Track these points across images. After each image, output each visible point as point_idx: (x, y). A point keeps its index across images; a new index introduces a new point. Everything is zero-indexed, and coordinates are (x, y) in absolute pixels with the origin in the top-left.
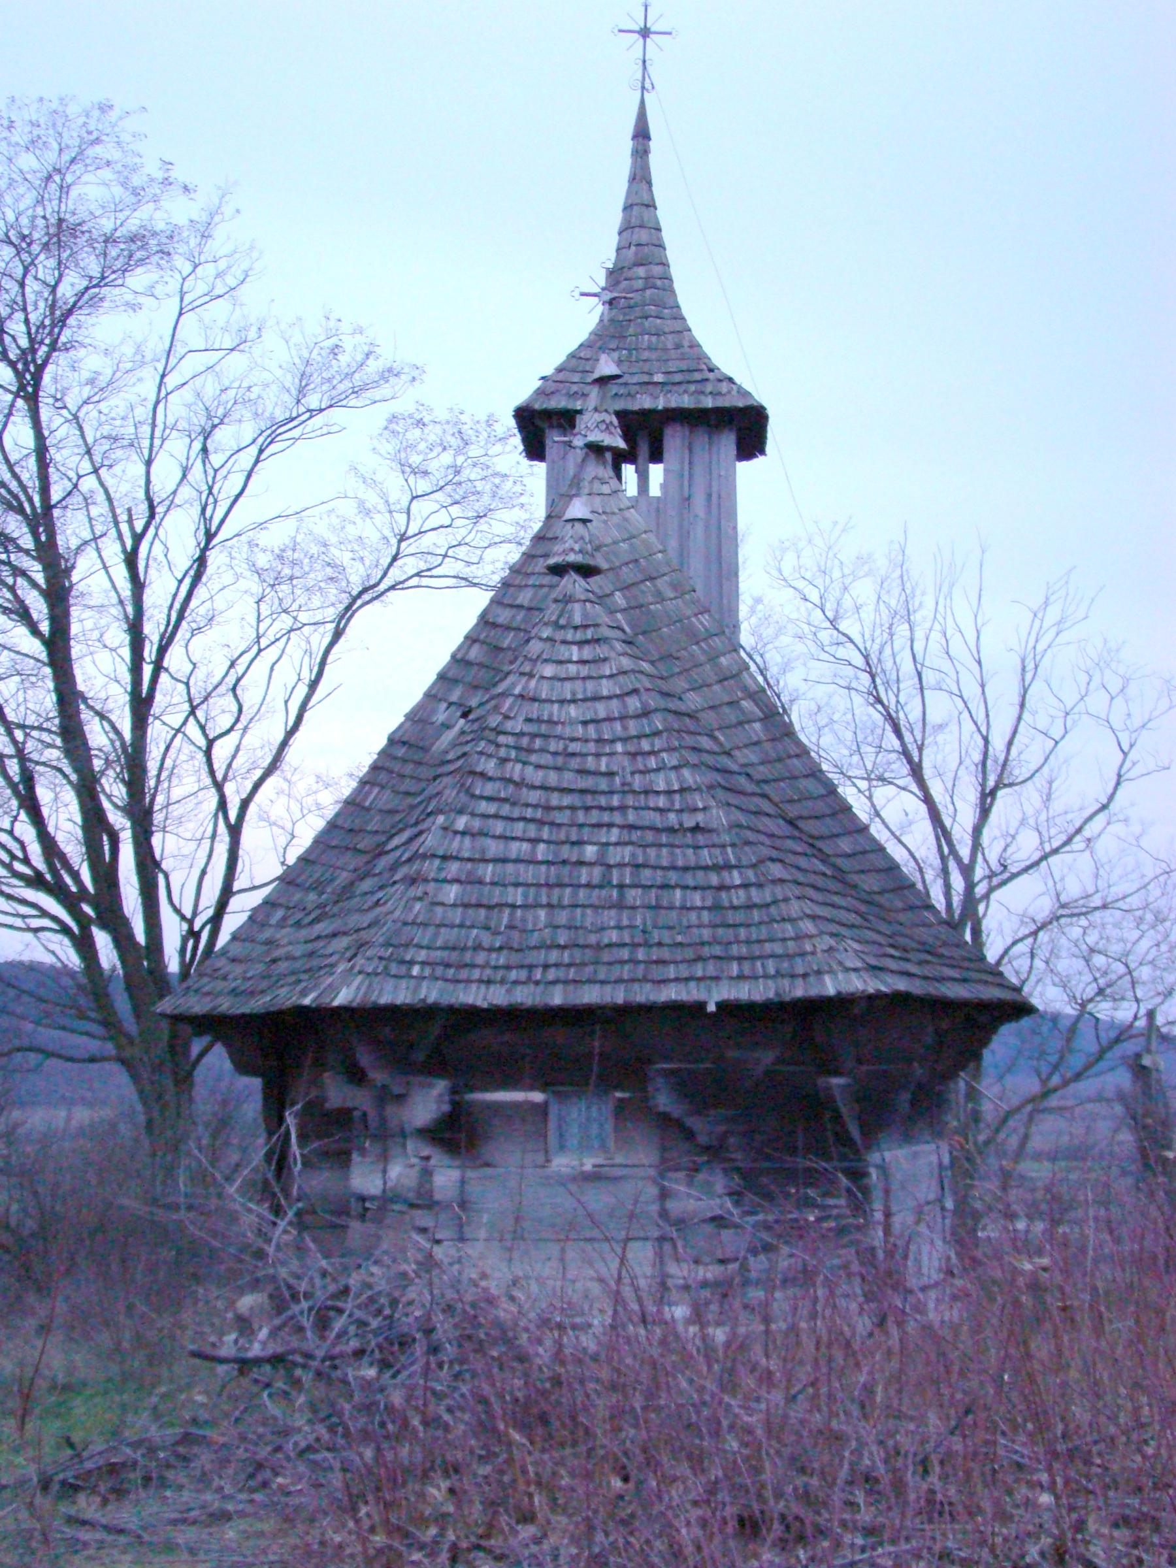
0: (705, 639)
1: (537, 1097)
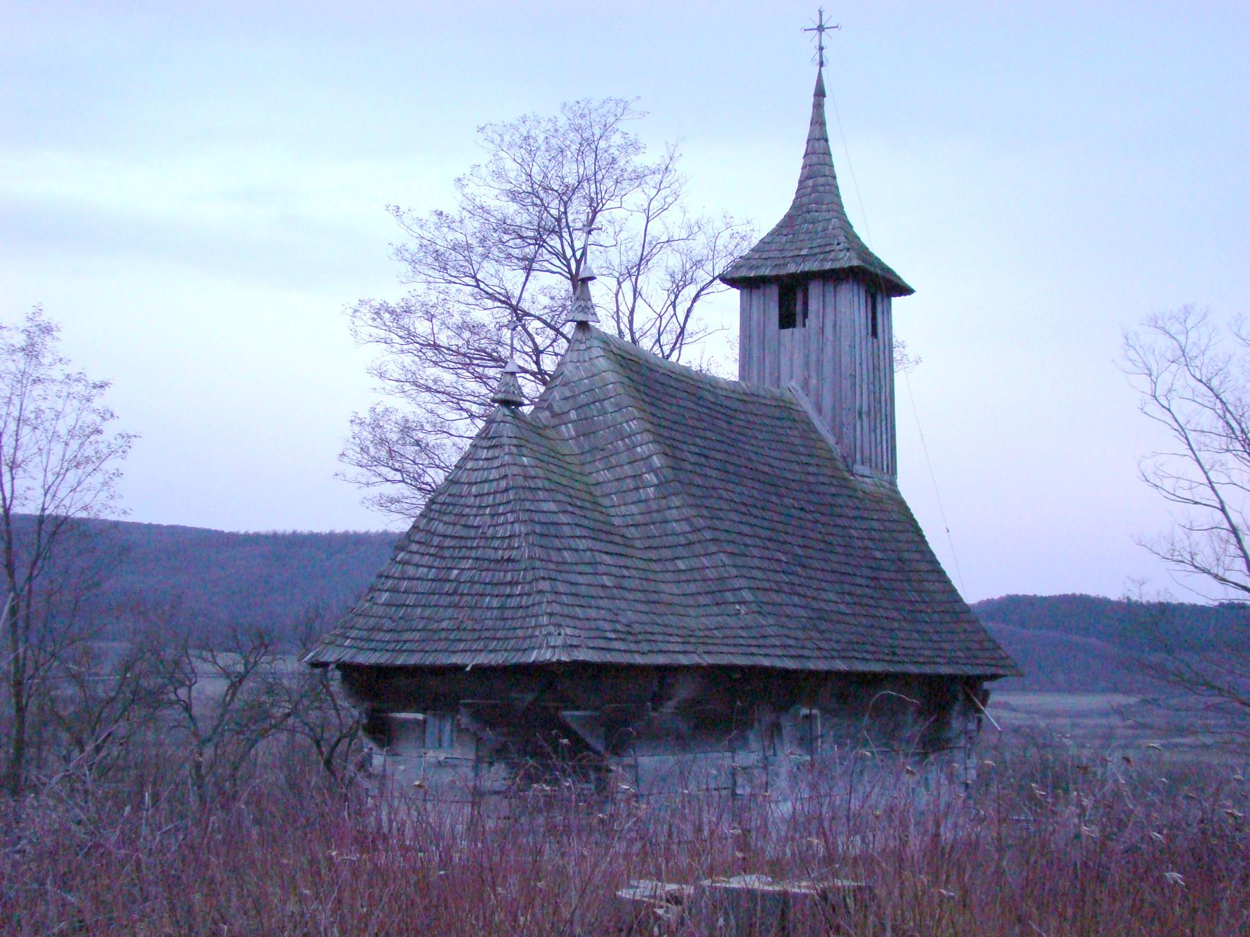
0: (629, 436)
1: (420, 716)
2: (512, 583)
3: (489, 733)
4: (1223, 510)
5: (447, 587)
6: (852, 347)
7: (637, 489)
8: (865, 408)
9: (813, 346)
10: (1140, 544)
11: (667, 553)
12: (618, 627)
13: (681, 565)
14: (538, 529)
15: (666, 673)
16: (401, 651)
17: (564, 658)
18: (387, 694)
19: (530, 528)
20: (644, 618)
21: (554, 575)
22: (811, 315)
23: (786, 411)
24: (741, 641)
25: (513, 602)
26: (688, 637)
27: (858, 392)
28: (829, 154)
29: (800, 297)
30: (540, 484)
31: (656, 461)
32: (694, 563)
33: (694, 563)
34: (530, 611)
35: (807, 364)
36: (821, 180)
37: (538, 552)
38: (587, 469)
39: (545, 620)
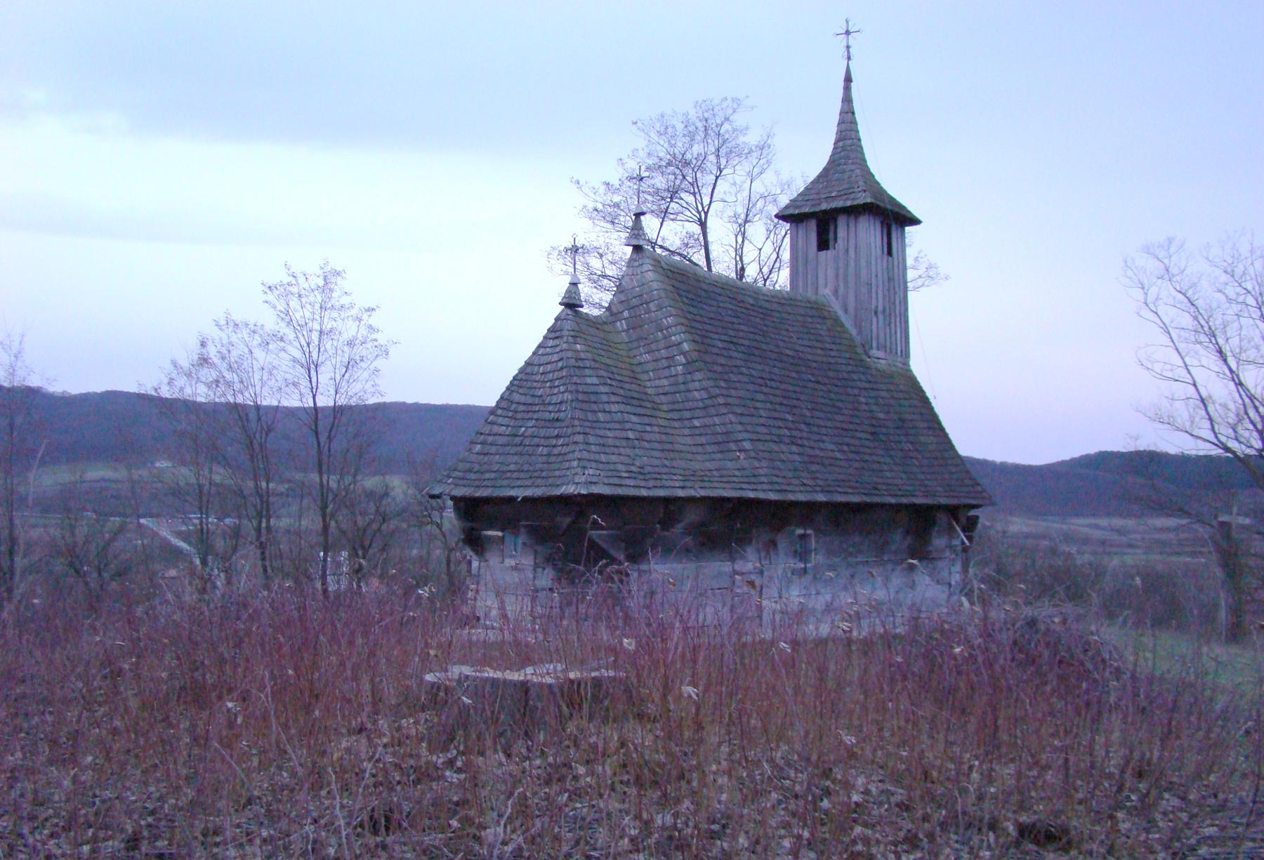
1: (500, 534)
2: (557, 437)
3: (539, 548)
4: (1195, 385)
5: (518, 440)
6: (869, 263)
7: (669, 367)
8: (880, 308)
9: (841, 265)
10: (1137, 411)
11: (687, 414)
12: (633, 469)
13: (696, 423)
14: (581, 397)
15: (670, 504)
16: (478, 487)
17: (584, 492)
18: (480, 517)
19: (574, 396)
20: (656, 462)
21: (588, 430)
22: (839, 241)
23: (819, 311)
24: (735, 479)
25: (556, 451)
26: (690, 476)
27: (874, 295)
28: (856, 123)
29: (832, 227)
30: (588, 364)
31: (686, 346)
32: (707, 421)
33: (707, 421)
34: (566, 458)
35: (837, 276)
36: (849, 142)
37: (578, 414)
38: (632, 354)
39: (575, 463)
